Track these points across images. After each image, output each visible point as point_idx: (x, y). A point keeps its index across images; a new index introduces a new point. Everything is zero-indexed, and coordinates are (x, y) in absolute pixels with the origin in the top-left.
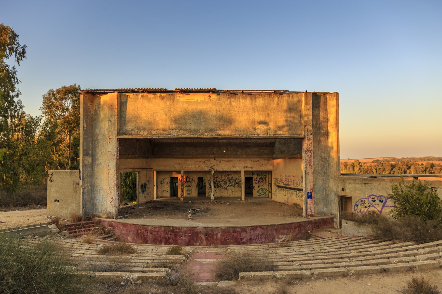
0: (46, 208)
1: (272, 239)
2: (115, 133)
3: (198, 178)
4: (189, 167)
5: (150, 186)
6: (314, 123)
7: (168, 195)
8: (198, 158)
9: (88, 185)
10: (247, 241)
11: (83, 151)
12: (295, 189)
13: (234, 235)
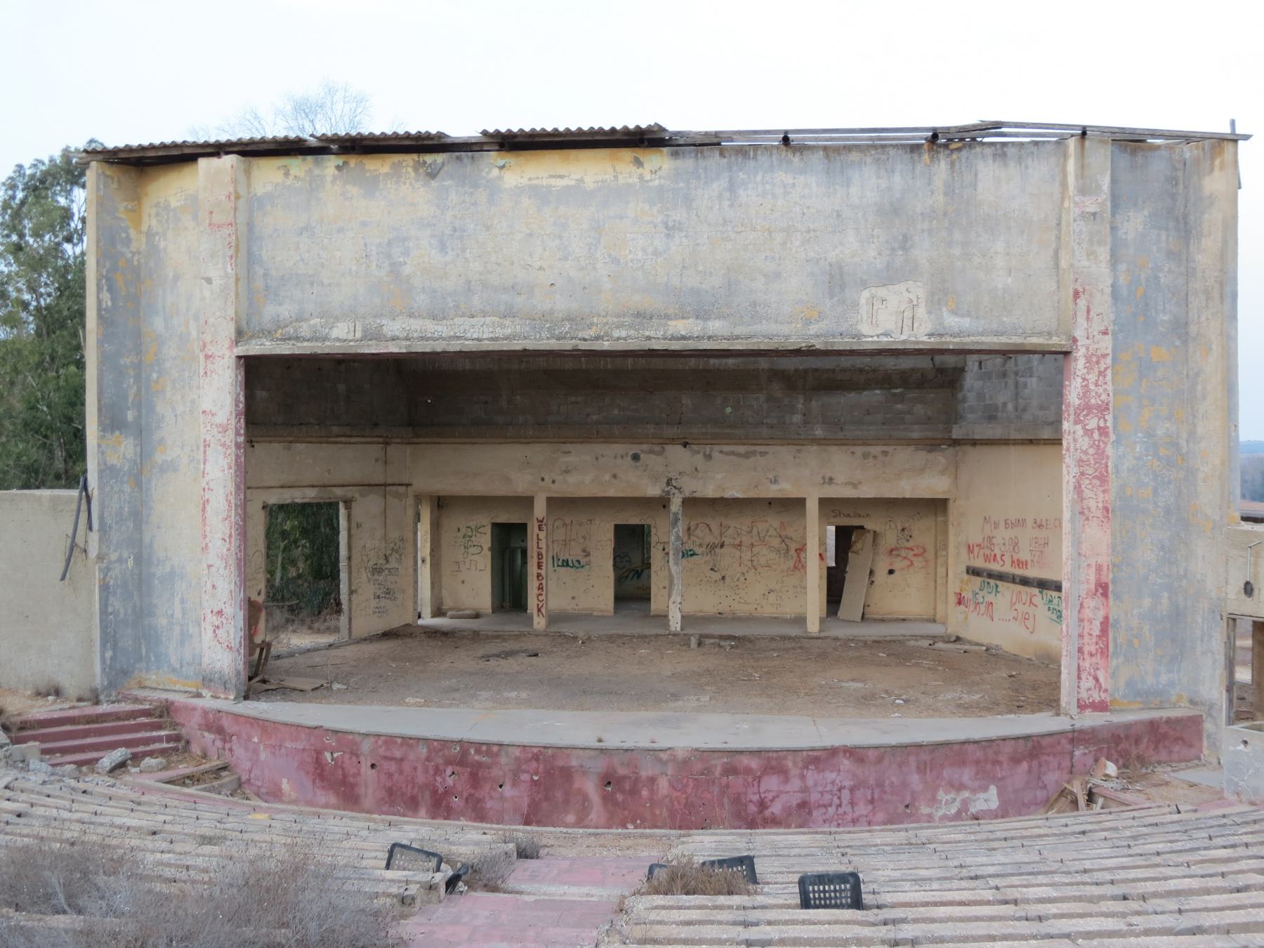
0: (649, 526)
1: (901, 808)
2: (230, 330)
3: (617, 527)
4: (572, 479)
5: (399, 561)
6: (1123, 280)
8: (609, 438)
9: (125, 555)
10: (788, 811)
11: (100, 410)
13: (727, 786)
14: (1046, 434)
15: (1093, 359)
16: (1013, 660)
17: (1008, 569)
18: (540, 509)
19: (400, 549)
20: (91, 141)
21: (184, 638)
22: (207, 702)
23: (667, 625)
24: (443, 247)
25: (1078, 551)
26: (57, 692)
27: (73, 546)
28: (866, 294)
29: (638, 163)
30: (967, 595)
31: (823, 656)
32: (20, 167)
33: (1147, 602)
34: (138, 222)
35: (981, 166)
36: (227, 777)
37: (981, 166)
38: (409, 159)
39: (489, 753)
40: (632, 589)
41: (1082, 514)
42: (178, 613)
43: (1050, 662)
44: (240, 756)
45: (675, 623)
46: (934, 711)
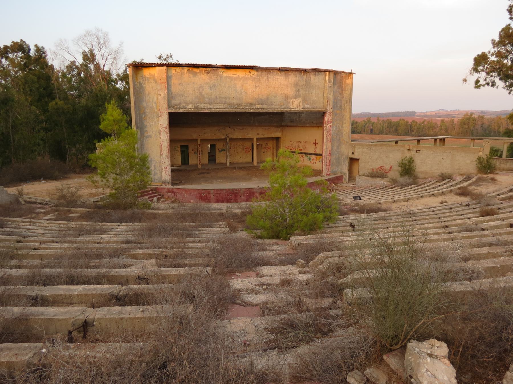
2: (166, 106)
4: (206, 135)
12: (306, 154)
15: (330, 113)
23: (226, 165)
24: (211, 89)
25: (327, 147)
29: (250, 72)
40: (212, 158)
41: (327, 141)
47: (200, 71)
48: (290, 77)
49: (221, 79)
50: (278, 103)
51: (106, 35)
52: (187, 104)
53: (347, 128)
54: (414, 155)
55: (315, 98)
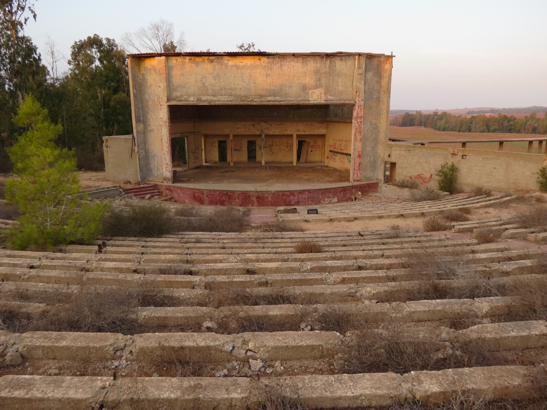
0: (255, 141)
2: (166, 99)
4: (239, 130)
6: (366, 88)
7: (217, 159)
14: (348, 121)
15: (360, 106)
16: (340, 171)
17: (339, 151)
18: (231, 138)
19: (198, 147)
20: (95, 35)
21: (158, 170)
22: (165, 184)
24: (215, 79)
25: (354, 148)
26: (130, 182)
27: (132, 150)
28: (311, 91)
29: (260, 60)
30: (329, 156)
31: (298, 171)
32: (76, 42)
33: (368, 159)
34: (140, 71)
35: (337, 62)
36: (173, 200)
37: (337, 62)
38: (206, 58)
39: (232, 193)
40: (252, 156)
41: (356, 140)
42: (156, 164)
43: (347, 171)
44: (175, 195)
45: (263, 163)
46: (323, 182)
47: (203, 60)
48: (309, 63)
49: (226, 68)
50: (293, 95)
51: (171, 25)
52: (189, 96)
53: (383, 125)
54: (459, 161)
55: (341, 88)
